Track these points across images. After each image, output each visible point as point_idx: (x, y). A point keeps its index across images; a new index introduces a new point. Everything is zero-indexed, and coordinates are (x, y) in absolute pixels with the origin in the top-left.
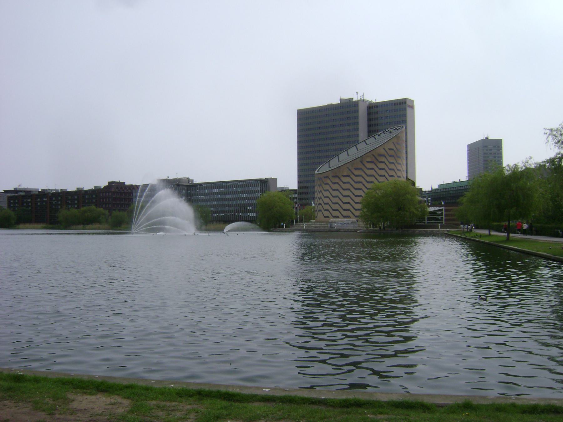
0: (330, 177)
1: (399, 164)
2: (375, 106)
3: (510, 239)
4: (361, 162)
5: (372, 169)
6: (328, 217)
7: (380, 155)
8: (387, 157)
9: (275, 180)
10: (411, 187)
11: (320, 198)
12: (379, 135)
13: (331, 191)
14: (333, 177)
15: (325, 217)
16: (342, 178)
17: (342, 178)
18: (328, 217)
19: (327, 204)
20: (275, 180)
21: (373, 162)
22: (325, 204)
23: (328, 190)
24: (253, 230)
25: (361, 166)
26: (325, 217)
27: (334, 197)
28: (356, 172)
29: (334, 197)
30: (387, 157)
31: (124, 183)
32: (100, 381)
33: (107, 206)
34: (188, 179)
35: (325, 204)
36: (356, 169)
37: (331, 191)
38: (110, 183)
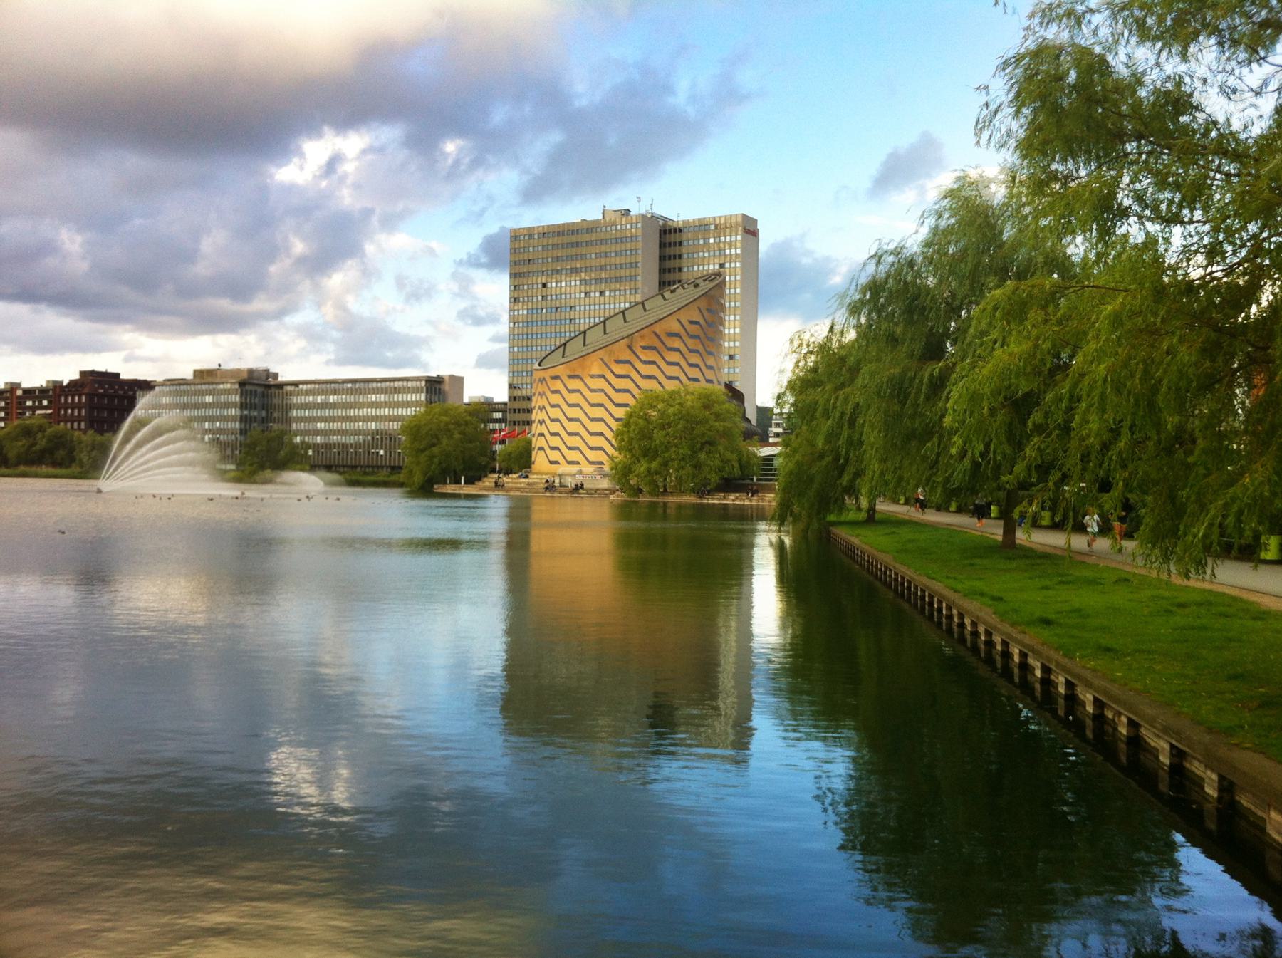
0: (565, 379)
1: (710, 353)
2: (675, 230)
3: (877, 516)
4: (630, 348)
5: (653, 363)
6: (556, 463)
7: (670, 335)
8: (685, 338)
9: (458, 381)
10: (732, 406)
11: (542, 422)
12: (673, 291)
13: (564, 407)
14: (571, 377)
15: (551, 463)
16: (590, 381)
17: (590, 381)
18: (556, 463)
19: (557, 434)
20: (458, 381)
21: (654, 348)
22: (552, 434)
23: (558, 406)
24: (206, 481)
25: (627, 355)
26: (551, 463)
27: (570, 420)
28: (619, 369)
29: (570, 420)
30: (685, 338)
31: (118, 375)
32: (799, 620)
33: (76, 425)
34: (267, 371)
35: (552, 434)
36: (618, 362)
37: (564, 407)
38: (83, 373)
